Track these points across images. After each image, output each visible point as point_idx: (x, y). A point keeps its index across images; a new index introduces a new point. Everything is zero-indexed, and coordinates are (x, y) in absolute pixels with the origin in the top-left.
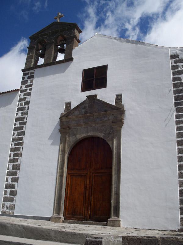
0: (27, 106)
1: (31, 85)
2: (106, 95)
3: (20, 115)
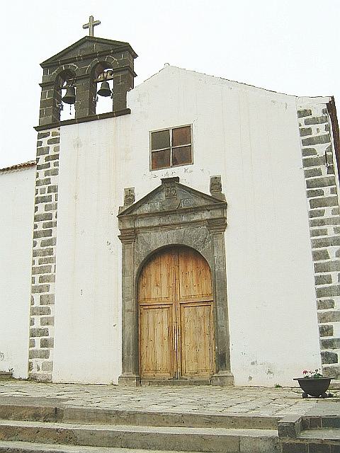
0: (53, 194)
1: (56, 157)
2: (194, 177)
3: (42, 211)
